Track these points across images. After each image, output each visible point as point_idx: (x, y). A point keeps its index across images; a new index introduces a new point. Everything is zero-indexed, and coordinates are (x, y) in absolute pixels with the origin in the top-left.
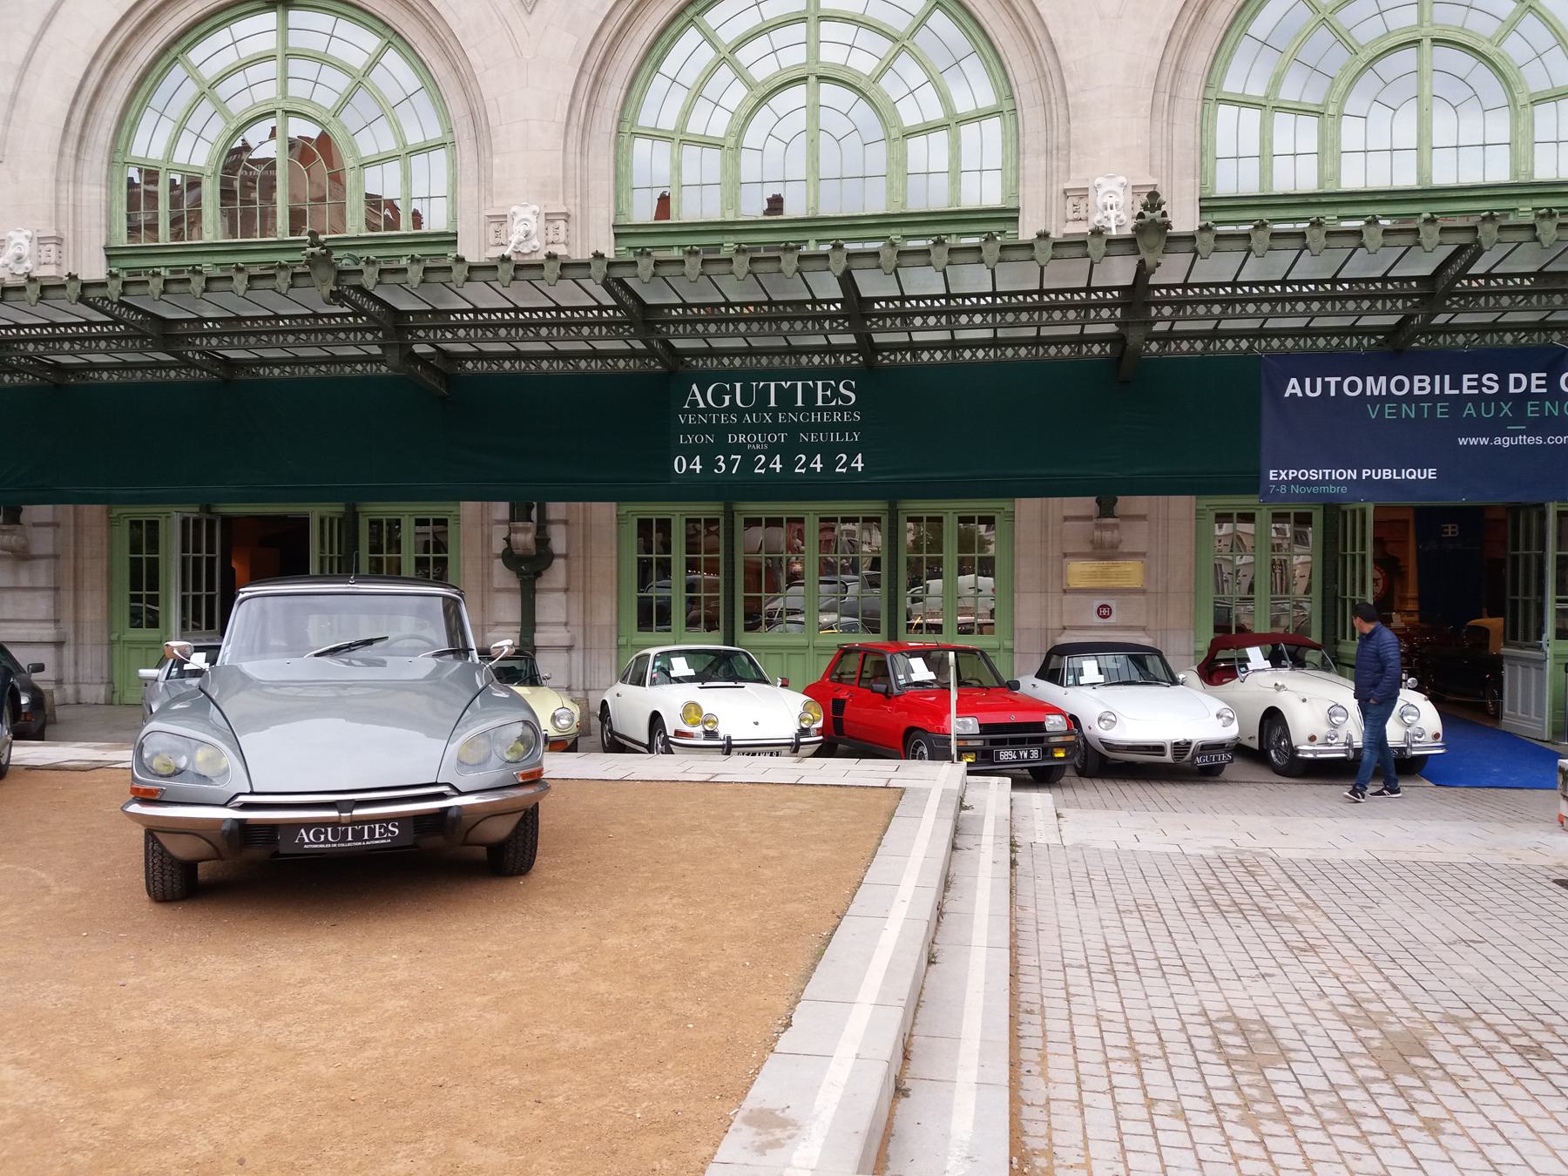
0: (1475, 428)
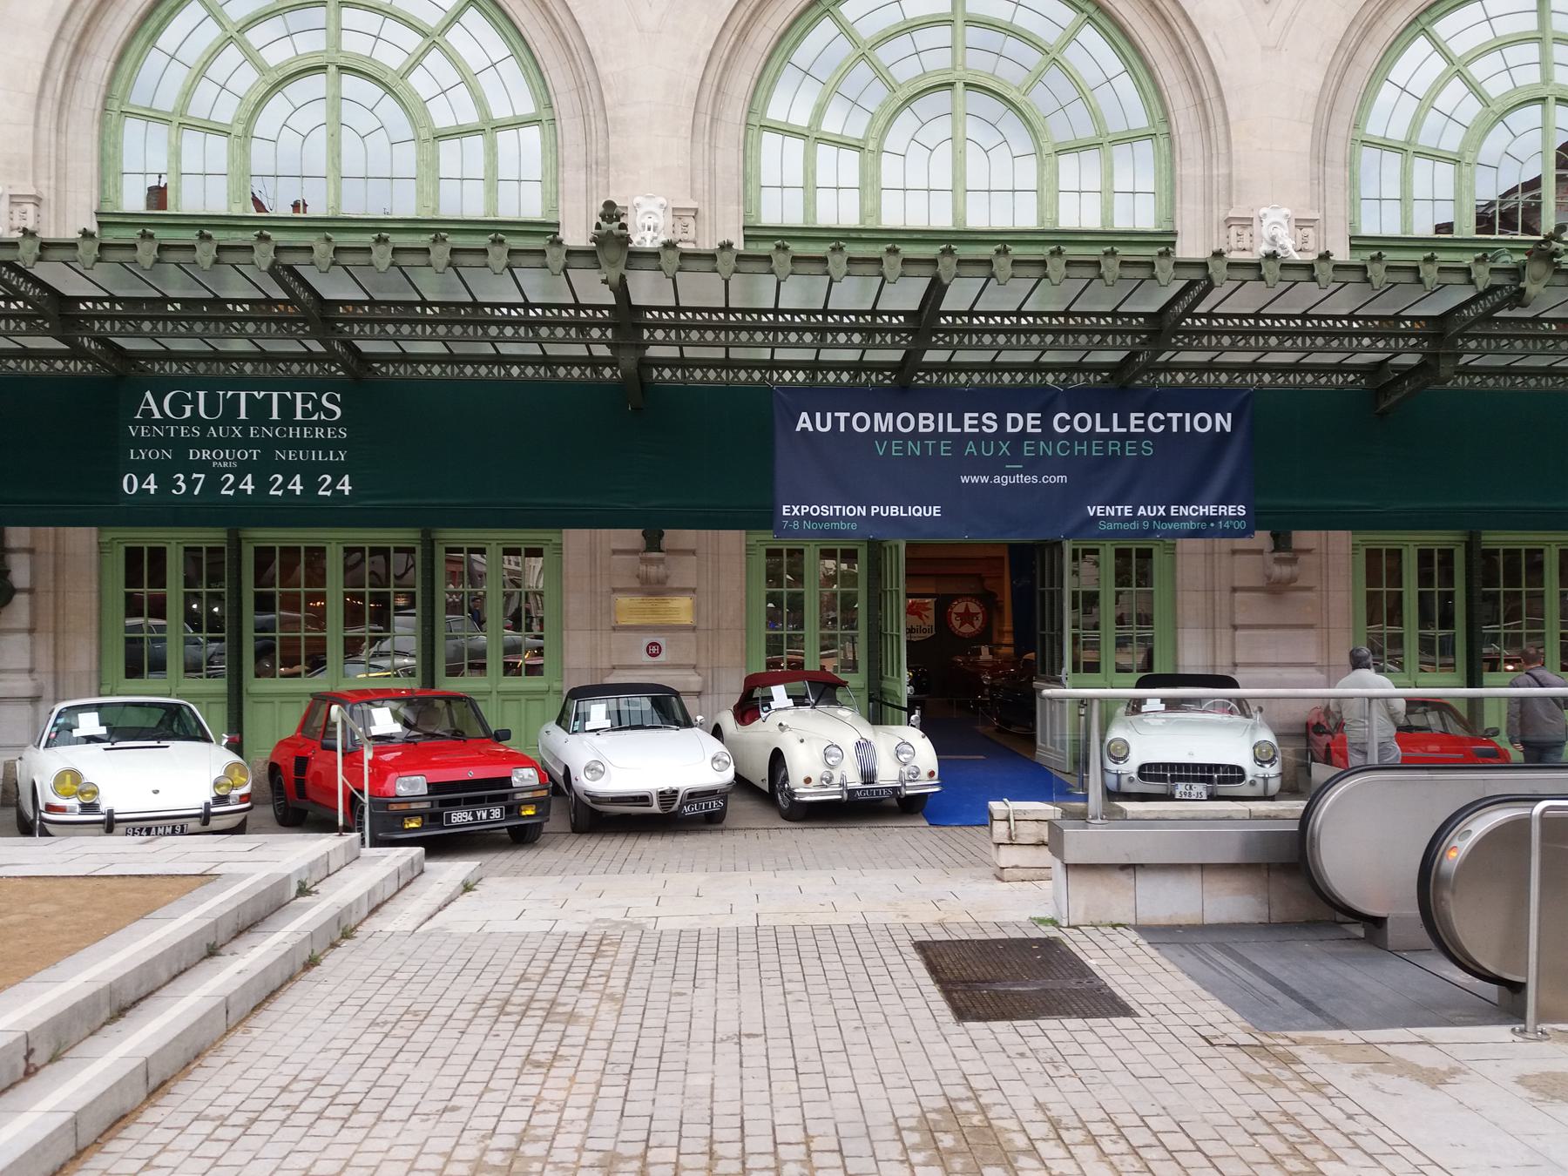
0: (978, 466)
